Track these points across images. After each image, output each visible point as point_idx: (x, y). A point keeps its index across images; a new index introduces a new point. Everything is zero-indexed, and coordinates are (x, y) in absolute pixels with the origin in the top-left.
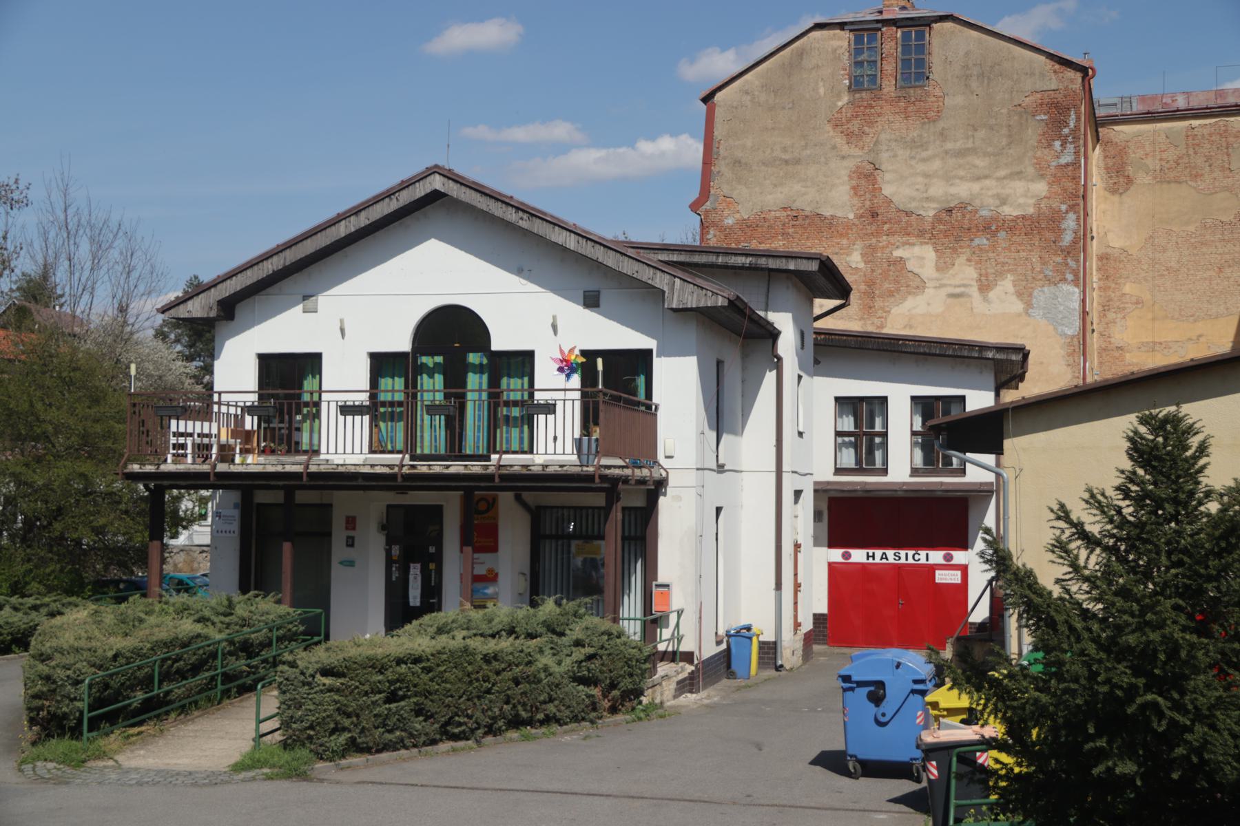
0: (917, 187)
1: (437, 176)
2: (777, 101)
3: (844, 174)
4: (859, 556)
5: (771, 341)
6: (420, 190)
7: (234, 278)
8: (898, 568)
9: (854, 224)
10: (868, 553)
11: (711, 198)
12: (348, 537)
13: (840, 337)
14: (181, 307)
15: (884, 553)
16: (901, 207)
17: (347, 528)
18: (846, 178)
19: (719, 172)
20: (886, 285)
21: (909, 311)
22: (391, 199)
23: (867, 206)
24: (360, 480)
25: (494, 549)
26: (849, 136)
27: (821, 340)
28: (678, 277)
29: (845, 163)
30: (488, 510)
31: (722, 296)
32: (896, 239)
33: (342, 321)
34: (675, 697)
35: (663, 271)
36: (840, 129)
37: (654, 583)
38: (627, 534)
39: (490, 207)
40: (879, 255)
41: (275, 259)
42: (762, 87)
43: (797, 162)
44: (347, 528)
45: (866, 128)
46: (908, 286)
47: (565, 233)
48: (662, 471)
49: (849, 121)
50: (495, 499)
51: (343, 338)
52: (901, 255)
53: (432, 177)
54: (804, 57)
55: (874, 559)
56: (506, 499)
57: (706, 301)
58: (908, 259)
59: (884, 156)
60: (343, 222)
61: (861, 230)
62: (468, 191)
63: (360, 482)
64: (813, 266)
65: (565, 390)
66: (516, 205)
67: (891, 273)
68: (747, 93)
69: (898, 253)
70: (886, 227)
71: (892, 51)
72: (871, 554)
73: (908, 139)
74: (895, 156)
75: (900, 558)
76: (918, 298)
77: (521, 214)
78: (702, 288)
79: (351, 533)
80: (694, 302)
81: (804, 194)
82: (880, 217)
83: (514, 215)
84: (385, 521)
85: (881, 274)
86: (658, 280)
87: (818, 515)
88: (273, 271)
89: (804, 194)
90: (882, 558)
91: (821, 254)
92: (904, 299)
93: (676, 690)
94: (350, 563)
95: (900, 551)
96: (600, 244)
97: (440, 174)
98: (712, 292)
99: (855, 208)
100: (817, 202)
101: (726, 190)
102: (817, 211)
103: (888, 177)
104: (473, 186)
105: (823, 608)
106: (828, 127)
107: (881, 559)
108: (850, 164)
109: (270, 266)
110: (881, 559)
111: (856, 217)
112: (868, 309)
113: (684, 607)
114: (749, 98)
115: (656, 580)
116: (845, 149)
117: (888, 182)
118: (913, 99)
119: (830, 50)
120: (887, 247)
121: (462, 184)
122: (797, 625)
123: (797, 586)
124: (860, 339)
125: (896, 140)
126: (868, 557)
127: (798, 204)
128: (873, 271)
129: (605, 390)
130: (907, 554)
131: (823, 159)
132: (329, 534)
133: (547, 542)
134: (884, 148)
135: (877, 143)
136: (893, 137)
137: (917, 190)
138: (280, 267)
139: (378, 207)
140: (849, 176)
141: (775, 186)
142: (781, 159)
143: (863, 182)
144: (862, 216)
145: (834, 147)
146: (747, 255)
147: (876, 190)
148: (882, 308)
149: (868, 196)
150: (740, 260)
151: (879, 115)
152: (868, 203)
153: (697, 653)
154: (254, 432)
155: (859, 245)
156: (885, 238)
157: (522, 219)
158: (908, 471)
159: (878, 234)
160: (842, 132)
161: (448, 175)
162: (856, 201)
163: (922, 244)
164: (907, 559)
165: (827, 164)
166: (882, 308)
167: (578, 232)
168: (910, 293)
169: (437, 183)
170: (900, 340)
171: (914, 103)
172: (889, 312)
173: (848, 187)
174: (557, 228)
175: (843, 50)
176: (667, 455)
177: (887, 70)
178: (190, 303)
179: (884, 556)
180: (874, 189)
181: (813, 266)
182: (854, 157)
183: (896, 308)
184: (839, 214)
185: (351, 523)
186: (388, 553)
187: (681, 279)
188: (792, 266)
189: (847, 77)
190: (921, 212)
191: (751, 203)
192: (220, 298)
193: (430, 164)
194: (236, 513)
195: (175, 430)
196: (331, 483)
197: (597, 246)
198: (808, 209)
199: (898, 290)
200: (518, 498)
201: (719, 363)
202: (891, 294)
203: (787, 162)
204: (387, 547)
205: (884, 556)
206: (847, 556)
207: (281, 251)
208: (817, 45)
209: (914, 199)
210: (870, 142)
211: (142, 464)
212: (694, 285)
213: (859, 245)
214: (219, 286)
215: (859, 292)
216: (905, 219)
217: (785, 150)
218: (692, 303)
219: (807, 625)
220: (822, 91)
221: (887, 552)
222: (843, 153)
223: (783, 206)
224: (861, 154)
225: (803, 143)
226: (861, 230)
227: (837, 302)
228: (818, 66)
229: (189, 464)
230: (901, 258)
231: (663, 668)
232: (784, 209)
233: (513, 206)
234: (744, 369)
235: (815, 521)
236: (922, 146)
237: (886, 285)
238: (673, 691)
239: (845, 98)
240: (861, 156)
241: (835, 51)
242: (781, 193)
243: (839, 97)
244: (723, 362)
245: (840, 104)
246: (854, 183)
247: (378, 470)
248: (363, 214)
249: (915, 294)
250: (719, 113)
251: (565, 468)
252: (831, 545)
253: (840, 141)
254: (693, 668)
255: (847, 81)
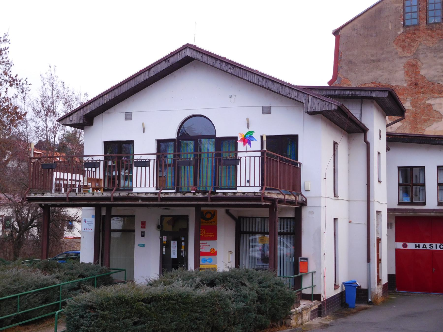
0: (438, 70)
1: (188, 49)
2: (369, 33)
3: (401, 65)
4: (411, 246)
5: (363, 135)
6: (180, 57)
7: (91, 104)
8: (432, 252)
9: (407, 89)
10: (416, 245)
11: (338, 79)
12: (142, 232)
13: (400, 137)
14: (68, 119)
15: (424, 245)
16: (430, 80)
17: (142, 228)
18: (403, 67)
19: (341, 67)
20: (423, 117)
21: (434, 129)
22: (166, 62)
23: (413, 80)
24: (140, 201)
25: (215, 238)
26: (404, 47)
27: (390, 138)
28: (311, 95)
29: (402, 60)
30: (211, 218)
31: (334, 104)
32: (428, 95)
33: (143, 124)
34: (311, 319)
35: (303, 93)
36: (399, 44)
37: (299, 258)
38: (202, 209)
39: (214, 63)
40: (419, 103)
41: (110, 94)
42: (362, 27)
43: (379, 60)
44: (142, 228)
45: (412, 44)
46: (434, 117)
47: (252, 75)
48: (303, 198)
49: (404, 40)
50: (215, 212)
51: (144, 132)
52: (430, 103)
53: (186, 50)
54: (382, 12)
55: (419, 248)
56: (221, 212)
57: (326, 107)
58: (434, 105)
59: (421, 56)
60: (143, 74)
61: (410, 91)
62: (204, 56)
63: (140, 202)
64: (385, 95)
65: (246, 152)
66: (227, 62)
67: (425, 111)
68: (354, 30)
69: (428, 102)
70: (422, 90)
71: (424, 7)
72: (417, 245)
73: (433, 48)
74: (427, 56)
75: (433, 247)
76: (440, 123)
77: (229, 66)
78: (324, 101)
79: (143, 230)
80: (319, 108)
81: (382, 76)
82: (419, 85)
83: (226, 67)
84: (160, 224)
85: (420, 112)
86: (300, 97)
87: (389, 225)
88: (110, 100)
89: (382, 76)
90: (423, 247)
91: (389, 88)
92: (432, 124)
93: (311, 315)
94: (143, 246)
95: (433, 244)
96: (270, 80)
97: (189, 48)
98: (329, 103)
99: (407, 81)
100: (389, 79)
101: (344, 75)
102: (388, 83)
103: (424, 66)
104: (206, 53)
105: (393, 272)
106: (394, 44)
107: (423, 248)
108: (405, 61)
109: (108, 97)
110: (423, 248)
111: (407, 86)
112: (415, 122)
113: (316, 271)
114: (355, 32)
115: (301, 256)
116: (402, 54)
117: (423, 69)
118: (435, 29)
119: (394, 8)
120: (423, 99)
121: (200, 52)
122: (379, 280)
123: (369, 260)
124: (410, 137)
125: (427, 49)
126: (416, 246)
127: (379, 80)
128: (416, 111)
129: (267, 151)
130: (436, 245)
131: (391, 59)
132: (134, 231)
133: (245, 235)
134: (421, 52)
135: (417, 50)
136: (425, 47)
137: (438, 72)
138: (113, 98)
139: (159, 66)
140: (404, 66)
141: (369, 72)
142: (371, 60)
143: (411, 69)
144: (410, 85)
145: (396, 53)
146: (350, 90)
147: (417, 73)
148: (421, 128)
149: (413, 75)
150: (347, 93)
151: (418, 37)
152: (413, 79)
153: (323, 295)
154: (101, 180)
155: (409, 98)
156: (422, 95)
157: (230, 69)
158: (437, 203)
159: (418, 93)
160: (400, 46)
161: (194, 48)
162: (407, 78)
163: (440, 97)
164: (436, 248)
165: (393, 61)
166: (421, 128)
167: (259, 74)
168: (434, 121)
169: (188, 53)
170: (431, 137)
171: (435, 31)
172: (424, 130)
173: (403, 72)
174: (248, 72)
175: (400, 8)
176: (306, 189)
177: (422, 16)
178: (71, 117)
179: (424, 246)
180: (416, 72)
181: (385, 95)
182: (406, 57)
183: (428, 128)
184: (399, 84)
185: (143, 224)
186: (161, 240)
187: (312, 96)
188: (374, 95)
189: (402, 20)
190: (440, 82)
191: (357, 81)
192: (85, 114)
193: (185, 43)
194: (93, 220)
195: (279, 231)
196: (126, 203)
197: (269, 81)
198: (384, 82)
199: (429, 119)
200: (227, 212)
201: (335, 144)
202: (425, 121)
203: (374, 61)
204: (161, 237)
205: (424, 246)
206: (405, 246)
207: (113, 90)
208: (388, 6)
209: (436, 76)
210: (414, 50)
211: (35, 194)
212: (319, 99)
213: (409, 98)
214: (85, 108)
215: (409, 121)
216: (432, 86)
217: (372, 55)
218: (318, 108)
219: (385, 280)
220: (390, 27)
221: (426, 244)
222: (401, 56)
223: (372, 81)
224: (409, 56)
225: (381, 52)
226: (410, 91)
227: (400, 117)
228: (388, 16)
229: (63, 194)
230: (430, 104)
231: (304, 304)
232: (373, 83)
233: (225, 62)
234: (349, 149)
235: (388, 228)
236: (440, 51)
237: (423, 117)
238: (310, 316)
239: (402, 30)
240: (410, 57)
241: (396, 8)
242: (371, 75)
243: (399, 29)
244: (337, 143)
245: (399, 33)
246: (406, 69)
247: (149, 196)
248: (152, 70)
249: (438, 121)
250: (341, 39)
251: (246, 194)
252: (397, 240)
253: (399, 50)
254: (321, 304)
255: (402, 22)
